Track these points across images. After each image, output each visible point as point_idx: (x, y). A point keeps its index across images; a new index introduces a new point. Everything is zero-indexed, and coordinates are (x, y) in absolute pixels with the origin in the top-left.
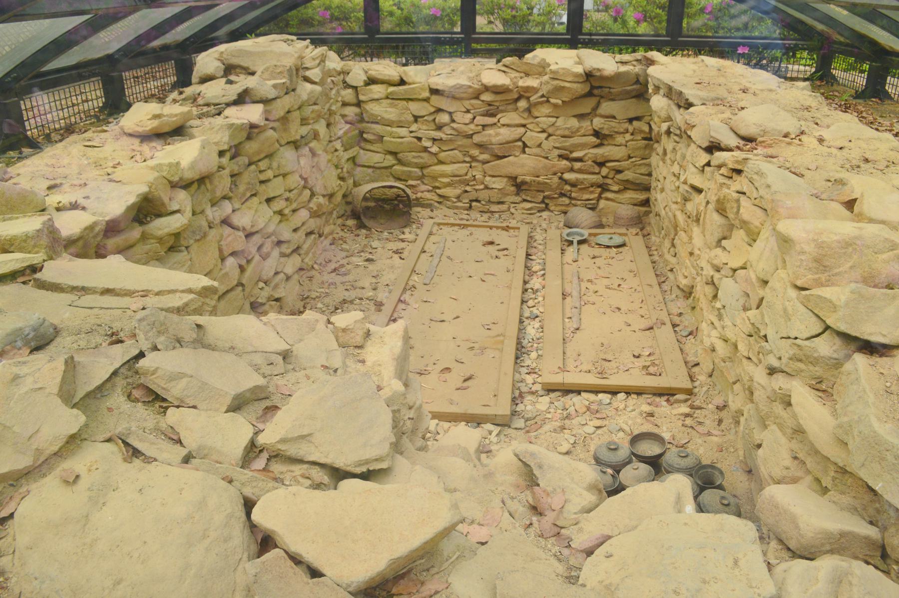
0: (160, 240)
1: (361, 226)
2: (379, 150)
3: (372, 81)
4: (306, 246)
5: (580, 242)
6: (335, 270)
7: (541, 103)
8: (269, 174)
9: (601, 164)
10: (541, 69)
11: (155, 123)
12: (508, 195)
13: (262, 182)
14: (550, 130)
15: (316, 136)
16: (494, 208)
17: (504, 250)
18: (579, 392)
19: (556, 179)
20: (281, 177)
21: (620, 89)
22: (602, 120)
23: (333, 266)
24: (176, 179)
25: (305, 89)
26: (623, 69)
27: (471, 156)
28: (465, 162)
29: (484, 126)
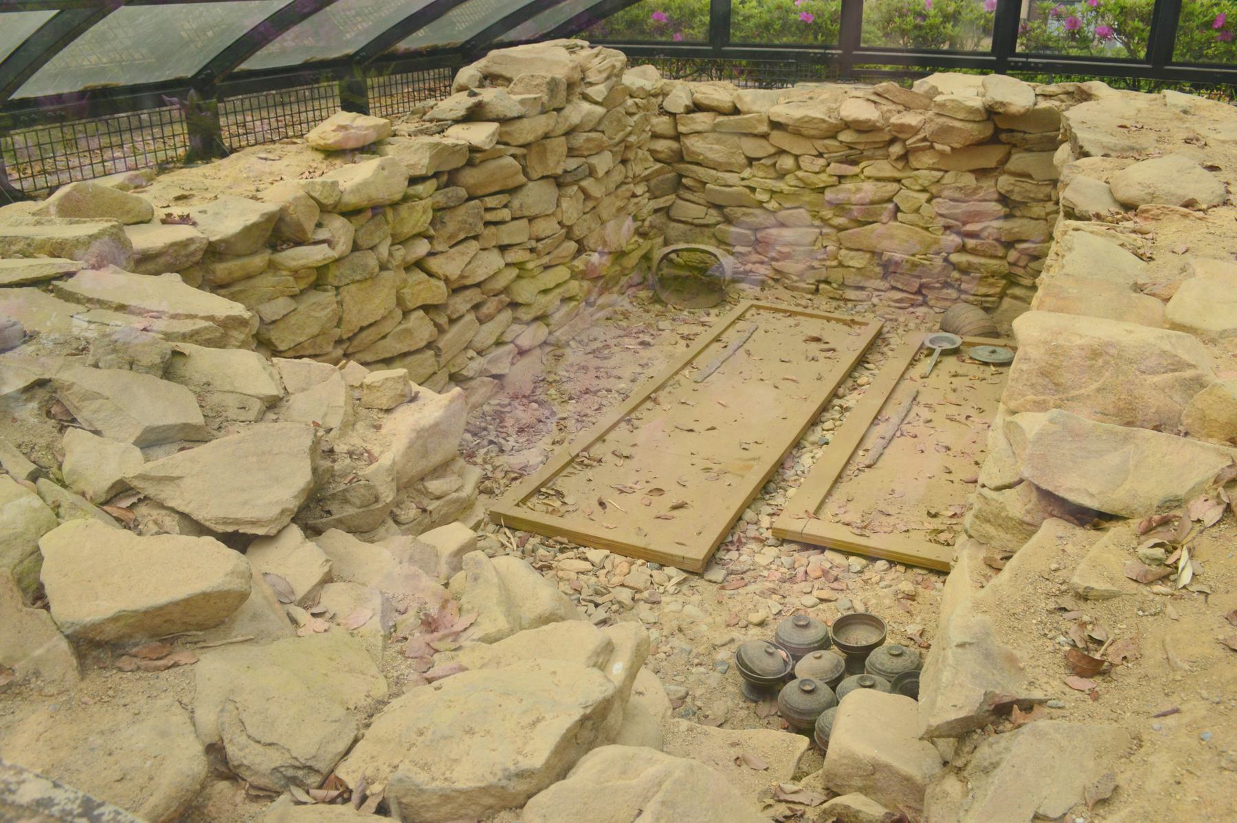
0: (295, 273)
1: (656, 300)
2: (701, 201)
3: (697, 107)
4: (557, 316)
5: (945, 353)
6: (594, 351)
7: (923, 149)
8: (505, 214)
9: (1009, 245)
10: (927, 101)
11: (340, 135)
12: (871, 278)
13: (487, 224)
14: (934, 190)
15: (592, 172)
16: (850, 294)
17: (829, 350)
18: (822, 549)
19: (938, 261)
20: (525, 221)
21: (1038, 135)
22: (1012, 179)
23: (595, 345)
24: (330, 201)
25: (579, 111)
26: (1043, 104)
27: (822, 220)
28: (812, 226)
29: (841, 178)
